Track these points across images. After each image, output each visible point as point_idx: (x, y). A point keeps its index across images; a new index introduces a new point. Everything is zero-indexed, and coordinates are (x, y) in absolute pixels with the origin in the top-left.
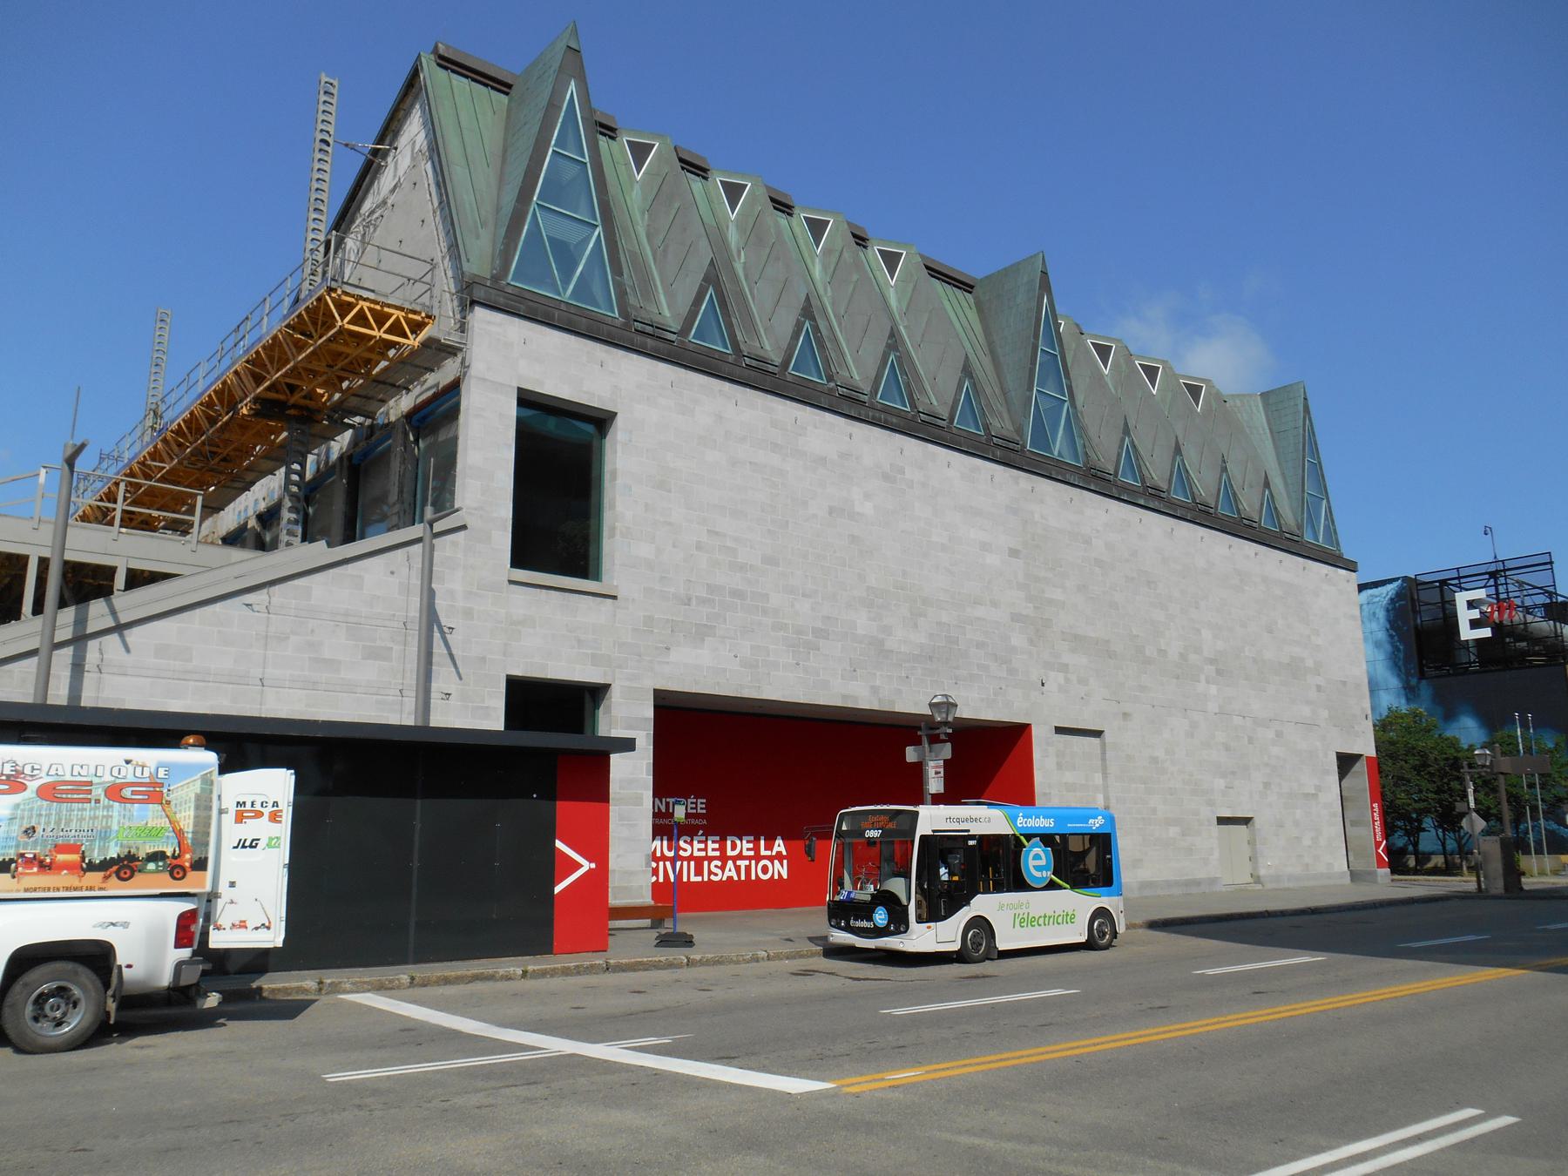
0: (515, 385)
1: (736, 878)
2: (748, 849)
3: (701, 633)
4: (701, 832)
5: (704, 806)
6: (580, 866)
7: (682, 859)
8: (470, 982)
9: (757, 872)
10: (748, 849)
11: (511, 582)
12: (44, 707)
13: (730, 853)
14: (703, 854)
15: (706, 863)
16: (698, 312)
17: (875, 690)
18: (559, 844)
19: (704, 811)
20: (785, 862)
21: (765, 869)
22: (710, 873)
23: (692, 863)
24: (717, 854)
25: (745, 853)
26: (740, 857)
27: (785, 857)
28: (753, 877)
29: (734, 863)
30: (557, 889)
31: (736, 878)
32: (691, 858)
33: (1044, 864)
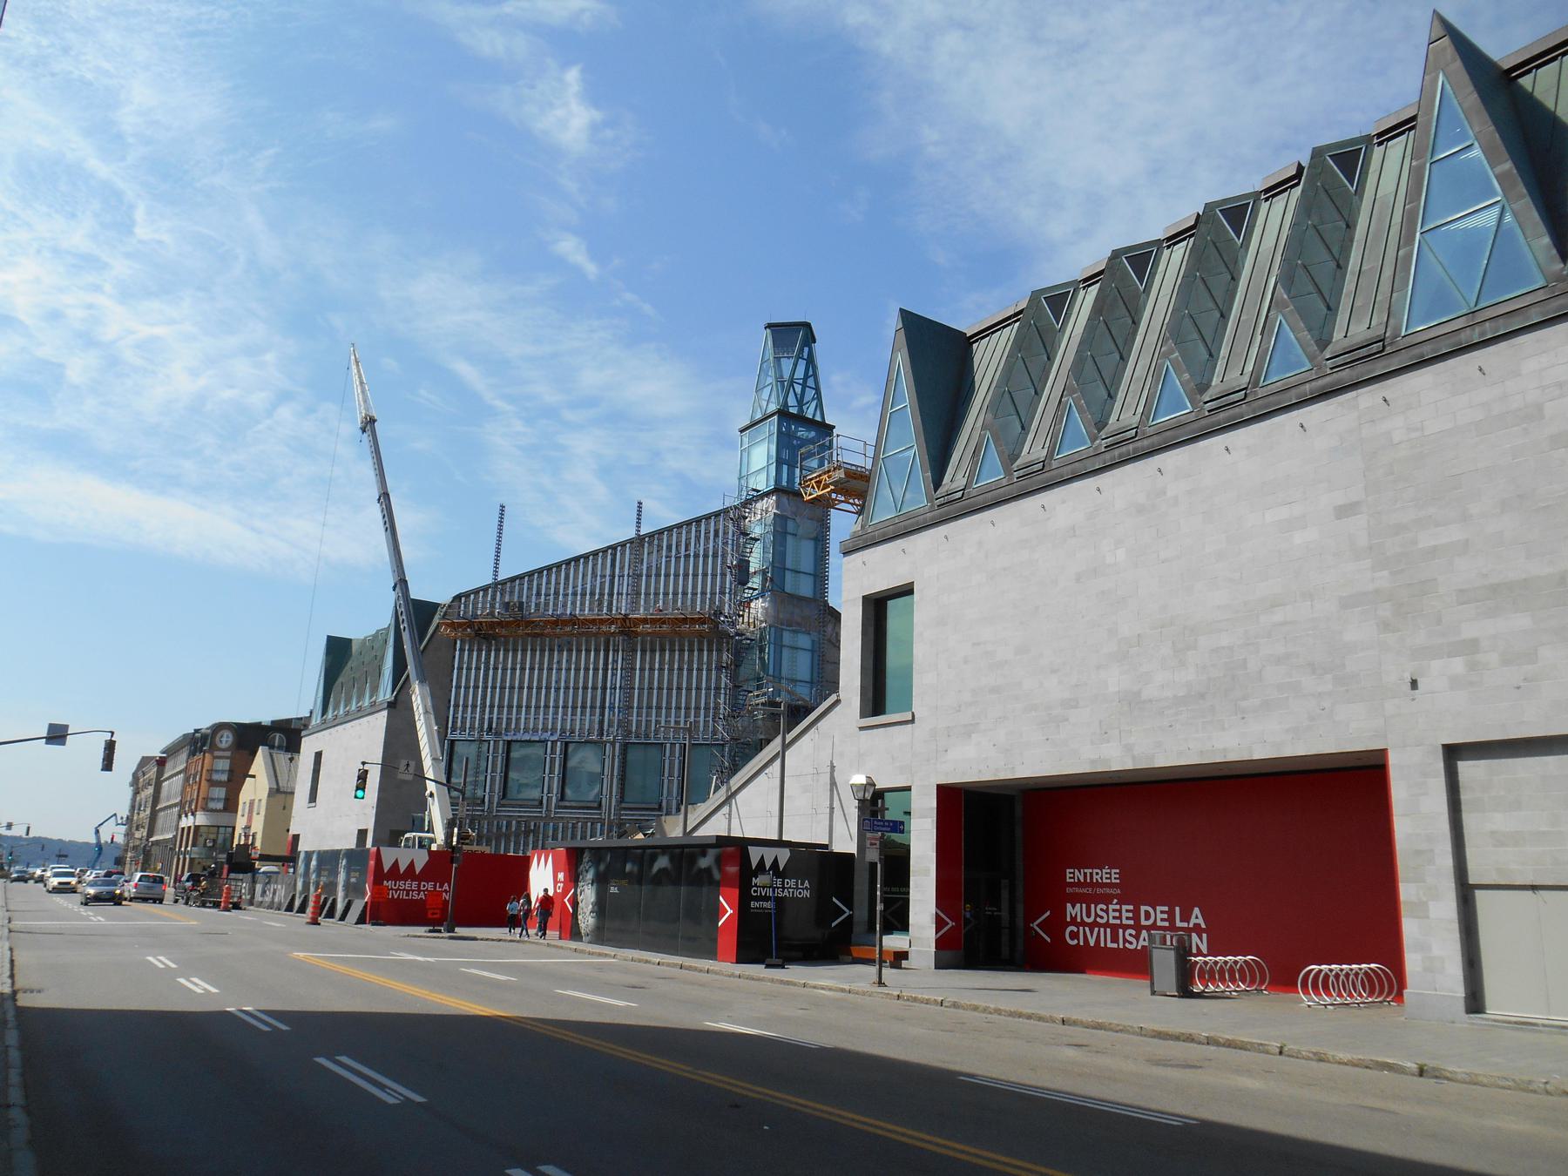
2: (1162, 920)
3: (969, 731)
4: (1115, 901)
5: (1117, 876)
7: (1100, 925)
9: (796, 894)
10: (1162, 920)
11: (861, 729)
13: (1144, 922)
14: (1118, 922)
15: (1121, 931)
16: (1432, 118)
17: (1128, 748)
18: (721, 898)
19: (1118, 881)
20: (1204, 936)
21: (800, 893)
22: (1125, 941)
23: (1108, 930)
24: (1131, 922)
25: (1159, 923)
26: (790, 888)
32: (404, 890)
33: (1177, 925)
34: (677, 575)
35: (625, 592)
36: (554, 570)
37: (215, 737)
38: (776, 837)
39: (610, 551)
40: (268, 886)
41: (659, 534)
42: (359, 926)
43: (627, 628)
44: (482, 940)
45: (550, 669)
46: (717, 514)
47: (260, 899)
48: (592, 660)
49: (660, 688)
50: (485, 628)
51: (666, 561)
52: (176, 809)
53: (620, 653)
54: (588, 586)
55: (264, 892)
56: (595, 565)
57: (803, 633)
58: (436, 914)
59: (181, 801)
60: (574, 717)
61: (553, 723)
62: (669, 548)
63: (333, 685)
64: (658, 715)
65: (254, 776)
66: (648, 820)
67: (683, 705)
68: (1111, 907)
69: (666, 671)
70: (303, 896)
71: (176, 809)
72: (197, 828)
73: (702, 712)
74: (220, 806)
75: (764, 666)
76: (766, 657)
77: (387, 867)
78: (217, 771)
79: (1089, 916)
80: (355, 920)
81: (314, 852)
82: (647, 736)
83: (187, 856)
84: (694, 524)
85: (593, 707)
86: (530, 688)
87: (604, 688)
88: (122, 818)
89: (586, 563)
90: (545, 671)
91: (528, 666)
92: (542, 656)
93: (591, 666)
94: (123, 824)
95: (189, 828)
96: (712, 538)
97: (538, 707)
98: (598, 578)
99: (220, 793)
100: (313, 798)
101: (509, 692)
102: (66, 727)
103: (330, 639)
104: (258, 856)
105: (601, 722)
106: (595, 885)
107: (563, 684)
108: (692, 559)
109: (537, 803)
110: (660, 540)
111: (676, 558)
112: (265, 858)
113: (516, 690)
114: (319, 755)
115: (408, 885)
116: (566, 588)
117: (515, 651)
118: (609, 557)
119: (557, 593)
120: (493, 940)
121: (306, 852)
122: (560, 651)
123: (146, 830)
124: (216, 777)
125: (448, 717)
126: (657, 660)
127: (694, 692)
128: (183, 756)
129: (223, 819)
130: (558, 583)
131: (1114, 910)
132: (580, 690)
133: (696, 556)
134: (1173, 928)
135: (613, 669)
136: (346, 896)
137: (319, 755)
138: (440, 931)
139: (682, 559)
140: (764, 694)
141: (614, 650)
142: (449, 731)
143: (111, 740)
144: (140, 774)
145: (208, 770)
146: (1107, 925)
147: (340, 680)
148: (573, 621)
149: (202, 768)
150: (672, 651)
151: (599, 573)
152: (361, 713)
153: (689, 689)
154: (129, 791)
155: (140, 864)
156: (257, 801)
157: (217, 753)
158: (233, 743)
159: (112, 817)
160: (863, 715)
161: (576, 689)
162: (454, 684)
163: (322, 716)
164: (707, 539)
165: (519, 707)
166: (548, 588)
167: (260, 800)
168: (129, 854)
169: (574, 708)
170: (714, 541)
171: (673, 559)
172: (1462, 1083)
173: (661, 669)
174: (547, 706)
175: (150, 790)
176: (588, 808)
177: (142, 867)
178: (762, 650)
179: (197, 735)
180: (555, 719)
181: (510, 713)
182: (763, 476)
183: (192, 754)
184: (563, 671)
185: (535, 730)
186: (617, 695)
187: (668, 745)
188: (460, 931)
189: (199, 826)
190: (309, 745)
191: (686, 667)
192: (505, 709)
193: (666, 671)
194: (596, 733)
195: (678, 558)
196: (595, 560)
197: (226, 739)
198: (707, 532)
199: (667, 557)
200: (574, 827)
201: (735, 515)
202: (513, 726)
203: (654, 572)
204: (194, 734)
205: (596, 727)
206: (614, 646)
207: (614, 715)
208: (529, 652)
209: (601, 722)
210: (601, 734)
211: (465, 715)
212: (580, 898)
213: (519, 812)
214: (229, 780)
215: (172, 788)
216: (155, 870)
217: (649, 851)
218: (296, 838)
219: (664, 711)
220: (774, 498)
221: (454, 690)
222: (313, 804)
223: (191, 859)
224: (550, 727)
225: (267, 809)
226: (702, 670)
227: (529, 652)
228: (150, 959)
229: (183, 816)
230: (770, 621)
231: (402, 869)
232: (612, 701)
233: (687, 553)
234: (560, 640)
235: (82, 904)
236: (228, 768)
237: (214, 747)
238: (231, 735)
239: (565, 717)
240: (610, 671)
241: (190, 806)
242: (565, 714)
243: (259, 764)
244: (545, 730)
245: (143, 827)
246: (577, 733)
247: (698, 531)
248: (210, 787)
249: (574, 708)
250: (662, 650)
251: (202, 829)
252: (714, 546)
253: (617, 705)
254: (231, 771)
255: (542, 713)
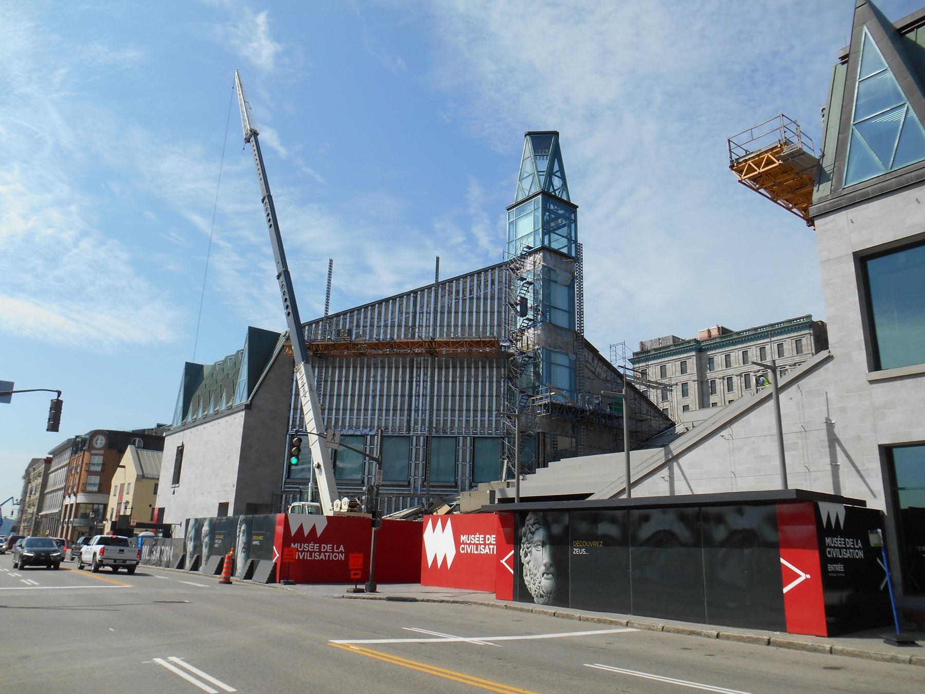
0: (850, 252)
1: (489, 553)
2: (493, 541)
6: (798, 576)
7: (305, 551)
8: (690, 634)
9: (332, 557)
10: (493, 541)
11: (872, 382)
12: (672, 496)
13: (322, 550)
14: (312, 550)
15: (313, 553)
18: (783, 561)
20: (344, 554)
22: (315, 557)
23: (475, 546)
24: (318, 550)
25: (328, 550)
26: (326, 552)
27: (344, 553)
28: (331, 559)
29: (324, 554)
30: (785, 590)
31: (489, 553)
32: (307, 551)
34: (464, 313)
35: (424, 324)
36: (370, 308)
37: (92, 441)
38: (900, 485)
39: (412, 295)
40: (155, 547)
41: (449, 282)
42: (269, 584)
43: (432, 348)
44: (422, 601)
45: (368, 382)
46: (500, 266)
47: (147, 558)
48: (400, 374)
49: (453, 396)
50: (321, 349)
51: (455, 302)
52: (62, 492)
53: (422, 369)
54: (396, 320)
55: (151, 552)
56: (401, 305)
57: (563, 354)
58: (358, 574)
59: (65, 486)
60: (387, 418)
61: (371, 422)
62: (457, 292)
63: (191, 397)
64: (453, 415)
65: (124, 467)
66: (447, 495)
67: (472, 408)
68: (476, 536)
69: (458, 383)
70: (195, 556)
71: (62, 492)
72: (78, 505)
73: (487, 413)
74: (95, 489)
75: (536, 374)
76: (541, 371)
77: (293, 531)
78: (94, 464)
79: (301, 548)
80: (214, 572)
81: (205, 519)
82: (444, 432)
83: (70, 525)
84: (476, 275)
85: (402, 410)
86: (353, 395)
87: (410, 396)
88: (17, 500)
89: (394, 303)
90: (364, 383)
91: (351, 379)
92: (362, 372)
93: (400, 379)
94: (18, 504)
95: (72, 505)
96: (489, 285)
97: (359, 410)
98: (404, 314)
99: (96, 479)
100: (176, 479)
101: (337, 399)
102: (11, 384)
103: (186, 362)
104: (135, 524)
105: (409, 421)
106: (548, 547)
107: (378, 393)
108: (475, 301)
109: (360, 482)
110: (451, 287)
111: (463, 300)
112: (141, 526)
113: (342, 397)
114: (180, 451)
115: (310, 547)
116: (379, 321)
117: (341, 368)
118: (412, 299)
119: (372, 325)
120: (434, 601)
121: (196, 520)
122: (376, 368)
123: (36, 507)
124: (93, 468)
125: (289, 418)
126: (451, 375)
127: (480, 398)
128: (68, 453)
129: (98, 498)
130: (372, 318)
131: (311, 546)
132: (392, 397)
133: (478, 298)
134: (333, 552)
135: (416, 381)
136: (247, 557)
137: (180, 451)
138: (361, 591)
139: (468, 301)
140: (547, 397)
141: (417, 368)
142: (290, 427)
143: (57, 399)
144: (31, 469)
145: (87, 464)
146: (474, 544)
147: (197, 393)
148: (391, 344)
149: (83, 461)
150: (462, 368)
151: (404, 310)
152: (218, 415)
153: (476, 396)
154: (22, 483)
155: (31, 532)
156: (126, 485)
157: (93, 452)
158: (104, 446)
159: (10, 499)
160: (870, 370)
161: (388, 396)
162: (294, 392)
163: (183, 420)
164: (486, 286)
165: (345, 410)
166: (365, 322)
167: (129, 484)
168: (23, 524)
169: (387, 410)
170: (492, 288)
171: (461, 301)
172: (876, 659)
173: (454, 382)
174: (366, 410)
175: (40, 480)
176: (400, 486)
177: (33, 533)
178: (536, 366)
179: (77, 439)
180: (372, 419)
181: (337, 414)
182: (531, 239)
183: (75, 452)
184: (378, 383)
185: (358, 427)
186: (421, 401)
187: (461, 438)
188: (385, 590)
189: (79, 504)
190: (171, 444)
191: (473, 380)
192: (334, 411)
193: (458, 383)
194: (405, 429)
195: (464, 300)
196: (401, 301)
197: (101, 442)
198: (486, 281)
199: (456, 299)
200: (390, 500)
201: (510, 268)
202: (340, 424)
203: (446, 310)
204: (75, 439)
205: (405, 424)
206: (417, 364)
207: (418, 416)
208: (351, 369)
209: (409, 421)
210: (409, 430)
211: (295, 416)
212: (524, 560)
213: (347, 489)
214: (103, 471)
215: (57, 478)
216: (44, 535)
217: (636, 513)
218: (162, 511)
219: (457, 412)
220: (541, 254)
221: (293, 397)
222: (177, 485)
223: (73, 527)
224: (369, 425)
225: (135, 490)
226: (485, 382)
227: (351, 369)
228: (159, 661)
229: (67, 496)
230: (542, 343)
231: (306, 533)
232: (417, 405)
233: (472, 296)
234: (375, 359)
235: (16, 566)
236: (101, 462)
237: (91, 447)
238: (103, 439)
239: (380, 417)
240: (414, 383)
241: (73, 489)
242: (380, 415)
243: (128, 457)
244: (365, 427)
245: (34, 506)
246: (390, 429)
247: (479, 281)
248: (88, 475)
249: (387, 410)
250: (454, 367)
251: (81, 506)
252: (491, 291)
253: (420, 408)
254: (104, 464)
255: (362, 415)
